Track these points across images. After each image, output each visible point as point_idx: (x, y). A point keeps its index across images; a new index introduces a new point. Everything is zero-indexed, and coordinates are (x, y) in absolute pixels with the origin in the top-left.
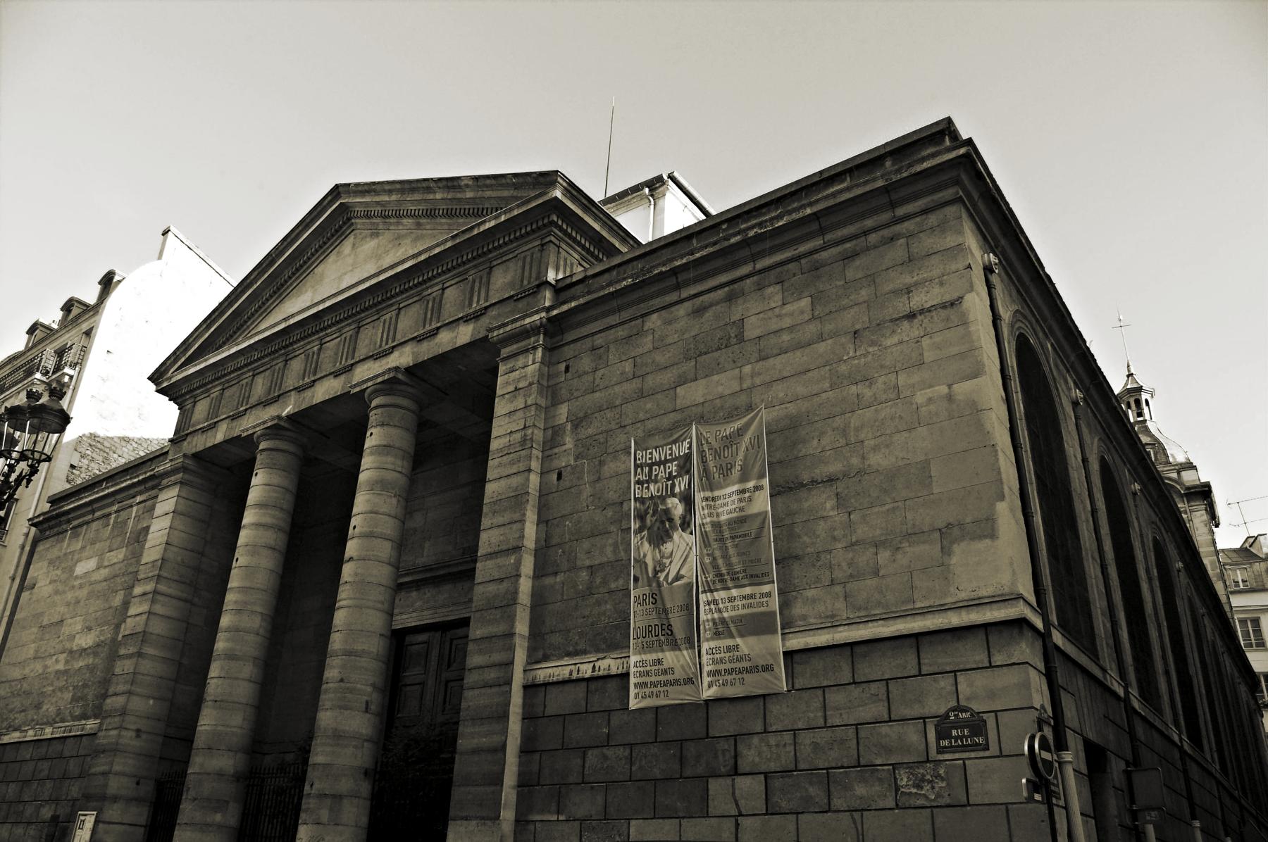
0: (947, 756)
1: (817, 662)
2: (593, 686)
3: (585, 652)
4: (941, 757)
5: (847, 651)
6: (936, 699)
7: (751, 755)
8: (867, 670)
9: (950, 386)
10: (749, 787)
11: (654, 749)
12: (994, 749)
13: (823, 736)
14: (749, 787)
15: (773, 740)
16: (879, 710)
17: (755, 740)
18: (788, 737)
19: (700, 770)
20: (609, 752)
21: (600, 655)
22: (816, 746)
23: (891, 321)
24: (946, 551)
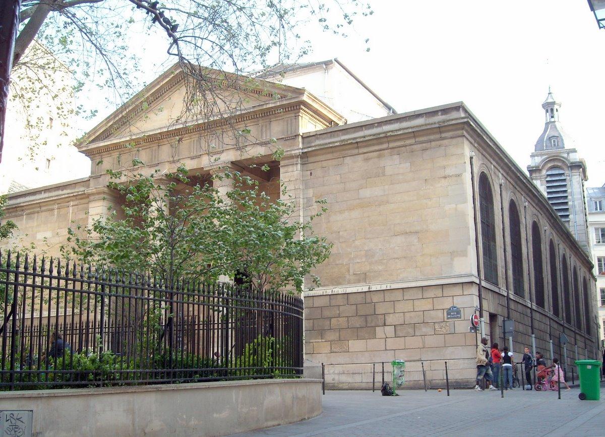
0: (449, 320)
1: (411, 291)
2: (332, 297)
3: (328, 285)
4: (448, 320)
5: (461, 285)
6: (447, 304)
7: (390, 319)
8: (430, 294)
9: (456, 205)
10: (390, 330)
11: (356, 318)
12: (462, 318)
13: (412, 314)
14: (390, 330)
15: (397, 315)
16: (430, 307)
17: (391, 315)
18: (402, 314)
19: (373, 324)
20: (340, 319)
21: (334, 287)
22: (411, 317)
23: (438, 178)
24: (452, 259)
